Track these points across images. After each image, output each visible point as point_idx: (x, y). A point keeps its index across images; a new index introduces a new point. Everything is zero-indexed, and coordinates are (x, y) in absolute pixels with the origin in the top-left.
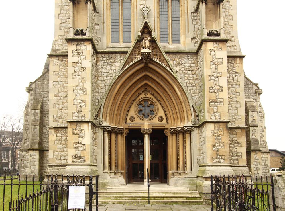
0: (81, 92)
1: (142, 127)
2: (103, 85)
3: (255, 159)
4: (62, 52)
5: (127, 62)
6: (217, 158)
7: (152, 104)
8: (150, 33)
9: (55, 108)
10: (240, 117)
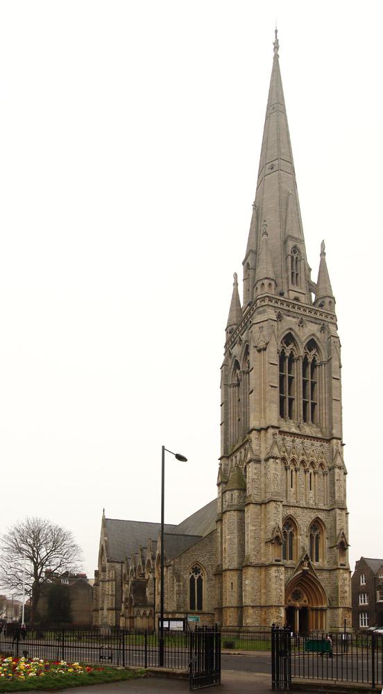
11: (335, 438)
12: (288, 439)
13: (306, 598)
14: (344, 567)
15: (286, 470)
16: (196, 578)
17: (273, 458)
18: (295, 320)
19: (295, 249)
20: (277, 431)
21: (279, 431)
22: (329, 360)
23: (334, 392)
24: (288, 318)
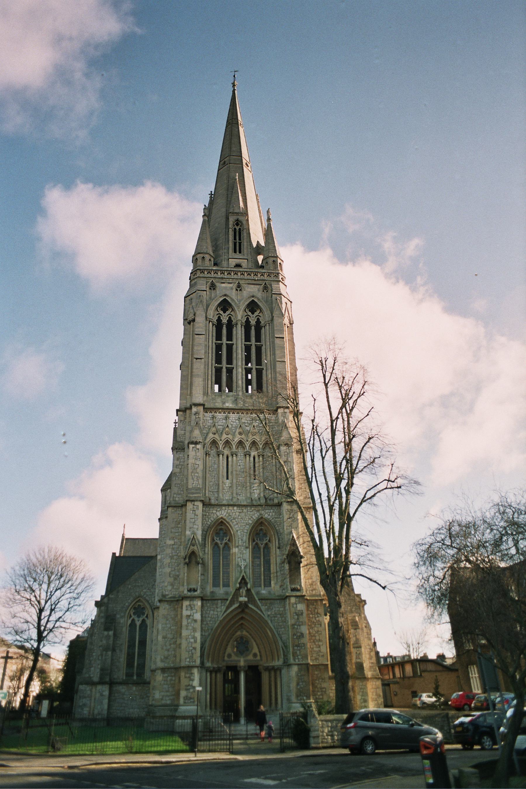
0: (192, 640)
1: (238, 665)
2: (206, 629)
3: (361, 689)
4: (171, 597)
5: (228, 608)
6: (300, 695)
7: (247, 642)
8: (246, 584)
9: (162, 649)
10: (322, 654)
11: (280, 407)
12: (220, 416)
13: (256, 650)
14: (298, 594)
15: (219, 455)
16: (138, 623)
17: (192, 443)
18: (231, 285)
19: (238, 222)
20: (201, 408)
21: (204, 408)
22: (272, 320)
23: (277, 352)
24: (223, 285)
